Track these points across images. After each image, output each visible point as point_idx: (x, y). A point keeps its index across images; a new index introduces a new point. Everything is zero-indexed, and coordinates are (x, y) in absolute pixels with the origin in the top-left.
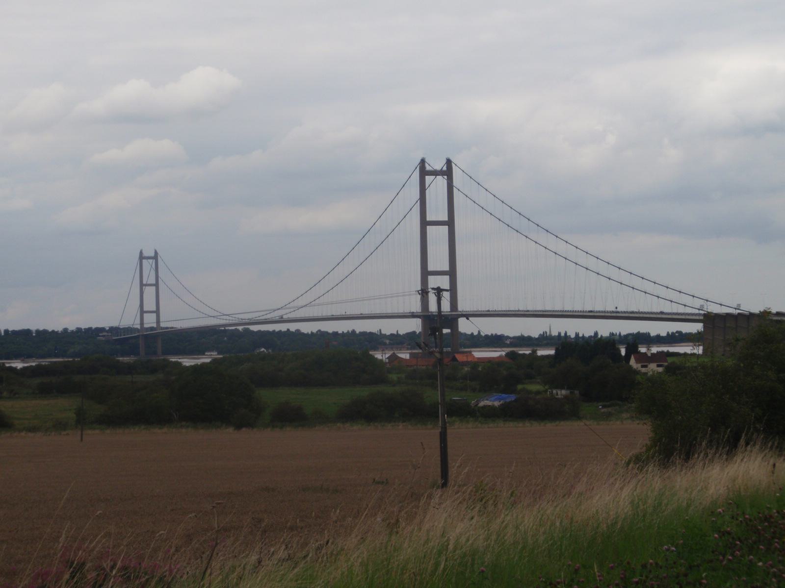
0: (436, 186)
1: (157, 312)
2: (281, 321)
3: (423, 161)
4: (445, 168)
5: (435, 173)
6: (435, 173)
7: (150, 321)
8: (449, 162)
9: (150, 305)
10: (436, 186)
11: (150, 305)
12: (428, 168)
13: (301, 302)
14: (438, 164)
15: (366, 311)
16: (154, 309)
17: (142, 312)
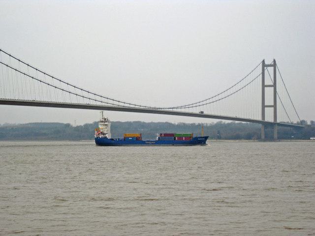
3: (263, 61)
8: (274, 61)
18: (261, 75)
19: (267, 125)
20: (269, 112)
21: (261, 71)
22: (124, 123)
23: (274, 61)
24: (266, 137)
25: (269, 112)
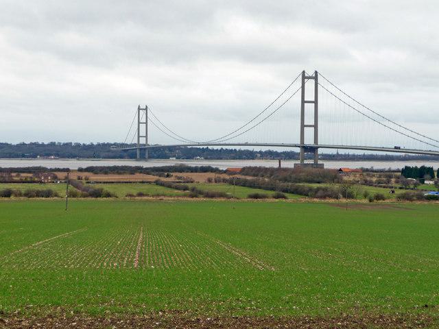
0: (310, 85)
1: (146, 137)
2: (246, 144)
3: (304, 72)
4: (314, 75)
5: (309, 78)
6: (309, 78)
7: (143, 141)
8: (316, 72)
9: (143, 133)
10: (310, 85)
11: (143, 133)
12: (306, 75)
13: (227, 138)
14: (310, 73)
15: (231, 143)
16: (313, 99)
17: (139, 137)
18: (301, 90)
19: (306, 148)
20: (309, 132)
21: (300, 85)
22: (281, 153)
23: (316, 72)
24: (140, 157)
25: (309, 132)
